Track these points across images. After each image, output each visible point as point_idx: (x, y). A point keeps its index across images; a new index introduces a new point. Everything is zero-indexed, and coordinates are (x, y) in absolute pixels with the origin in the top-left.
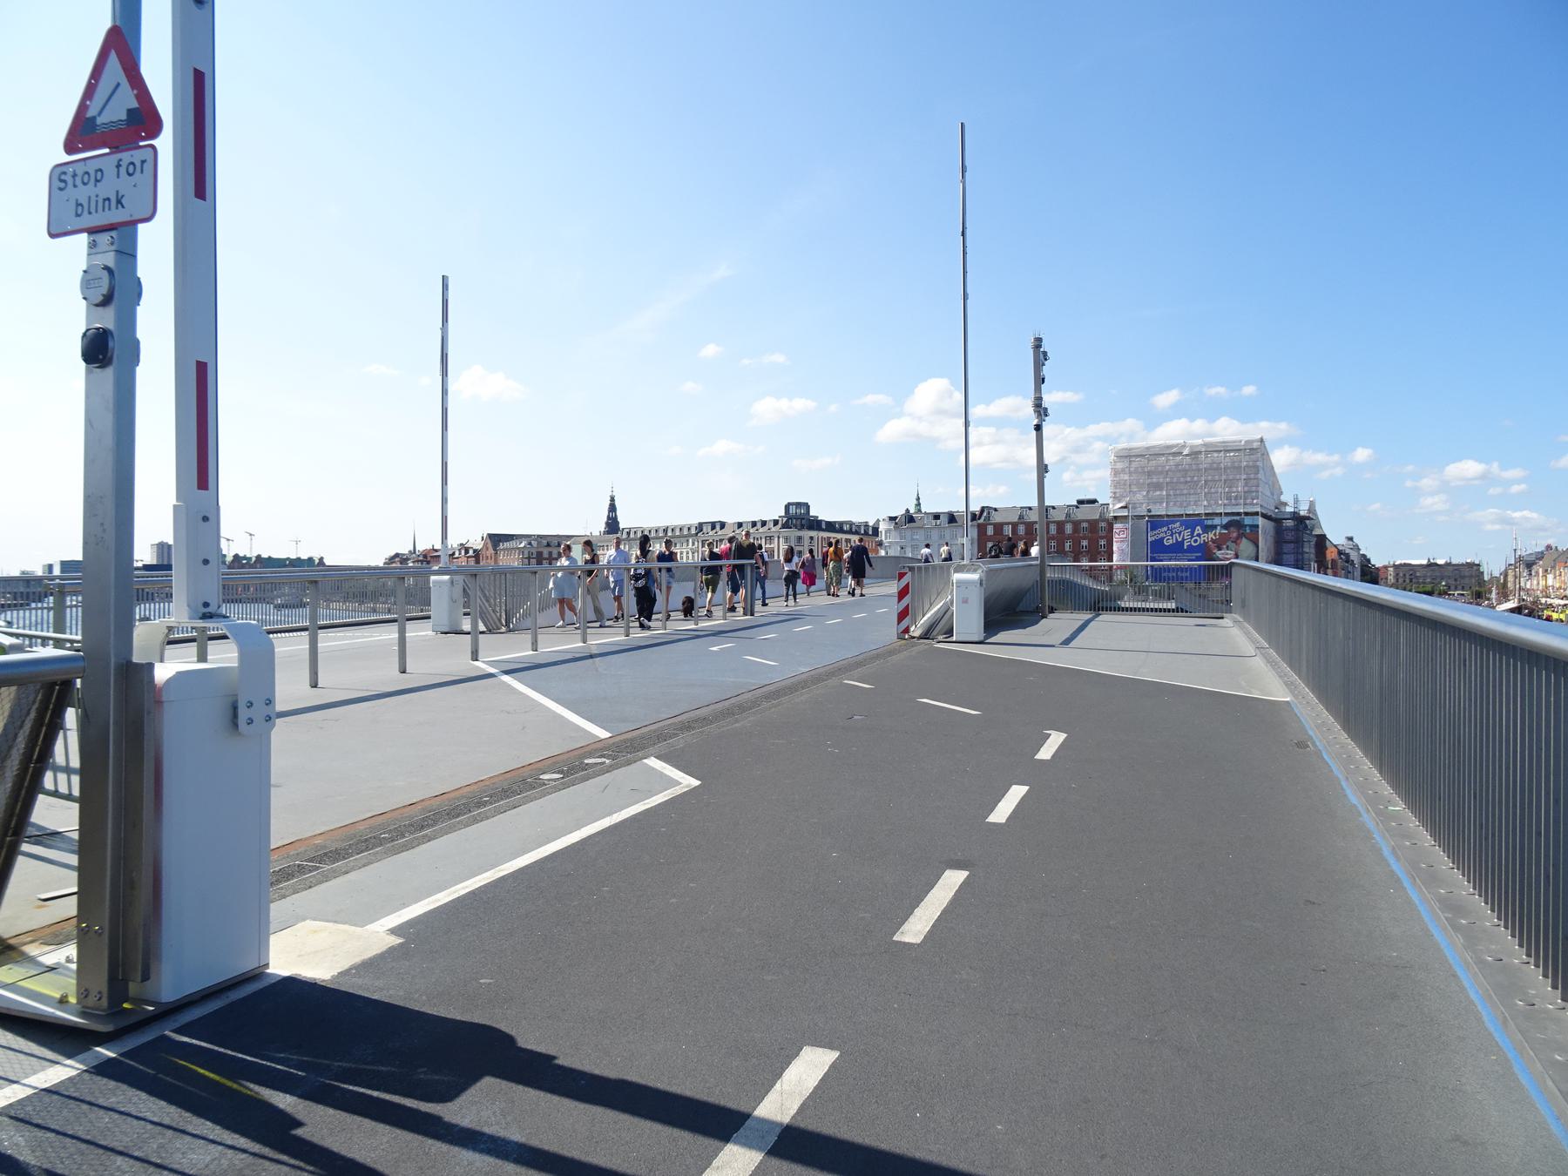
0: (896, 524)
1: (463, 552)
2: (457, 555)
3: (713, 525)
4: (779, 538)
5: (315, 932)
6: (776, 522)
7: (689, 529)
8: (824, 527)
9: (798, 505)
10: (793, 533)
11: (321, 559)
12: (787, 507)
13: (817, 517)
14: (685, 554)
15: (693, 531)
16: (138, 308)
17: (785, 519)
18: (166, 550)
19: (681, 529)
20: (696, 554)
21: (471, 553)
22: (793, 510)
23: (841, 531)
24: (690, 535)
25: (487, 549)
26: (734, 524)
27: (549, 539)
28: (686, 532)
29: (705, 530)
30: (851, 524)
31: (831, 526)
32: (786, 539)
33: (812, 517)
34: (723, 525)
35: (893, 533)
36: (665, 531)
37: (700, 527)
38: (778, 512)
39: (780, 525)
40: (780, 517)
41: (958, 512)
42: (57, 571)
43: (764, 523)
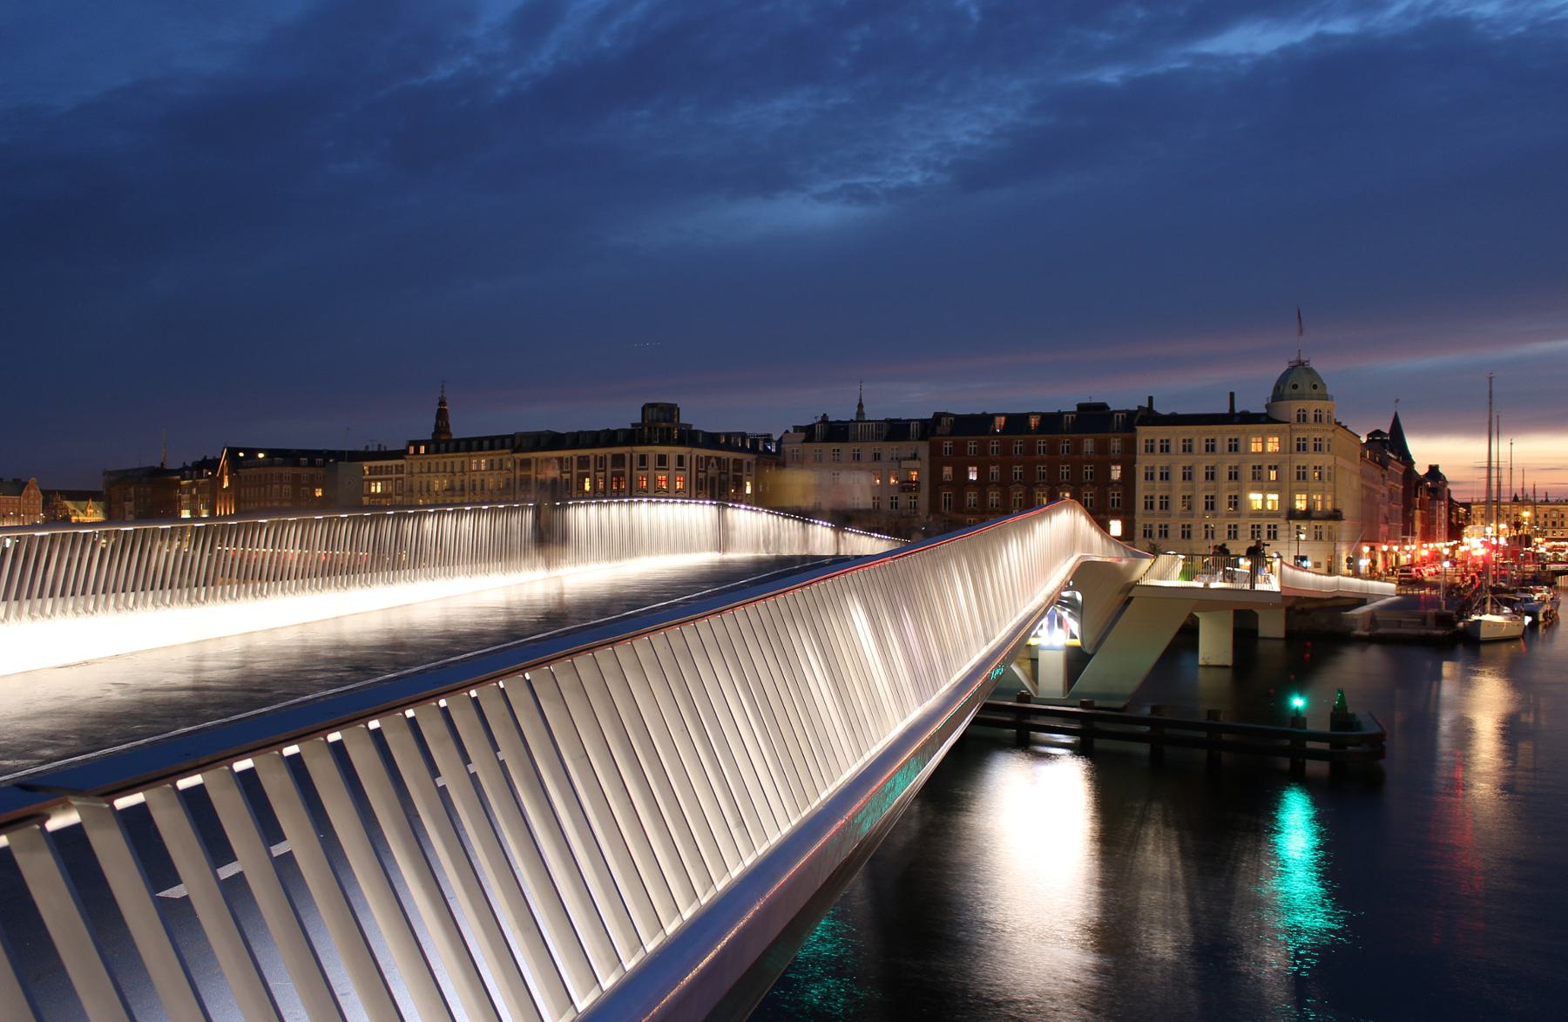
11: (1059, 411)
13: (691, 426)
23: (728, 446)
30: (744, 436)
31: (712, 440)
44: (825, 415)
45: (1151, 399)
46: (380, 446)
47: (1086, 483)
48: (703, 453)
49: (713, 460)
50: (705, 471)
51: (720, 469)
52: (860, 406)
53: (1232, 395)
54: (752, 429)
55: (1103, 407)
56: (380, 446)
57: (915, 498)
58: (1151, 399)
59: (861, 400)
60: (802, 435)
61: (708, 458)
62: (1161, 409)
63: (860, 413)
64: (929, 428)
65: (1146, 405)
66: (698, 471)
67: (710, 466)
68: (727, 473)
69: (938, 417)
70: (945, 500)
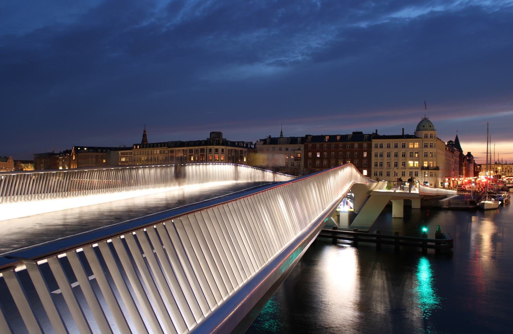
13: (226, 139)
23: (238, 146)
31: (233, 144)
36: (247, 144)
44: (270, 136)
45: (376, 130)
46: (124, 146)
47: (355, 158)
48: (230, 148)
49: (233, 151)
50: (231, 154)
51: (235, 153)
52: (282, 133)
53: (403, 129)
54: (246, 140)
55: (361, 133)
56: (124, 146)
57: (299, 163)
58: (376, 130)
59: (282, 131)
60: (262, 142)
62: (380, 134)
63: (281, 135)
64: (304, 140)
65: (375, 133)
66: (228, 154)
67: (232, 152)
68: (238, 155)
69: (307, 136)
70: (309, 163)
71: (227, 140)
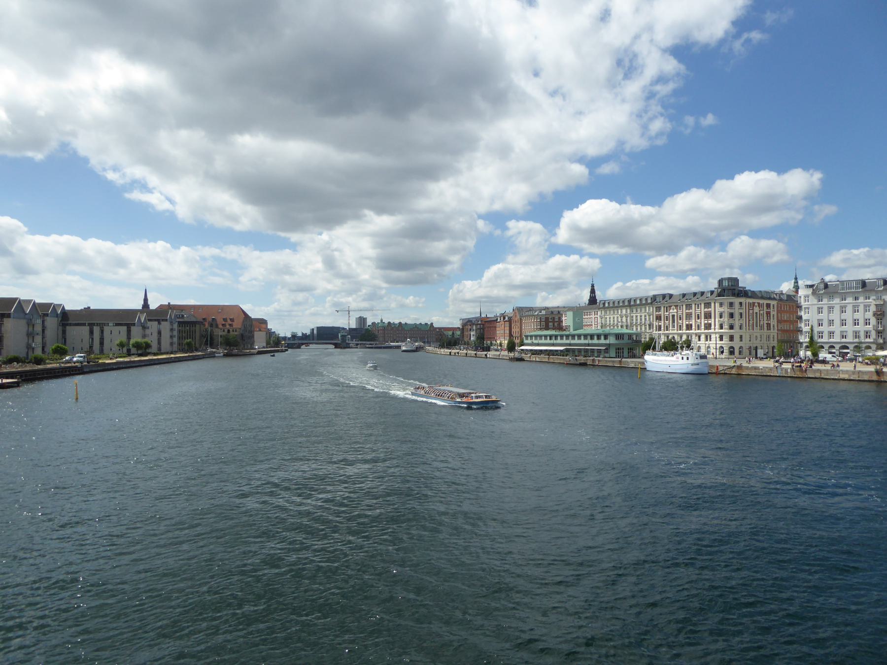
0: (813, 290)
1: (502, 318)
2: (499, 320)
3: (664, 296)
4: (715, 303)
5: (77, 399)
6: (712, 292)
7: (619, 302)
8: (750, 295)
9: (730, 279)
10: (727, 300)
11: (432, 324)
12: (720, 282)
13: (745, 288)
14: (616, 318)
15: (649, 301)
16: (91, 308)
17: (720, 290)
18: (362, 321)
19: (640, 300)
20: (652, 316)
21: (507, 318)
22: (725, 284)
23: (762, 298)
24: (647, 304)
25: (516, 316)
26: (680, 295)
27: (552, 310)
28: (644, 302)
29: (658, 300)
32: (721, 305)
33: (741, 287)
34: (671, 296)
35: (811, 297)
36: (629, 301)
37: (654, 298)
38: (713, 285)
39: (715, 294)
40: (715, 288)
41: (869, 279)
42: (315, 332)
43: (702, 293)
48: (751, 301)
49: (756, 304)
50: (753, 310)
61: (754, 303)
66: (749, 309)
67: (755, 307)
71: (747, 289)
